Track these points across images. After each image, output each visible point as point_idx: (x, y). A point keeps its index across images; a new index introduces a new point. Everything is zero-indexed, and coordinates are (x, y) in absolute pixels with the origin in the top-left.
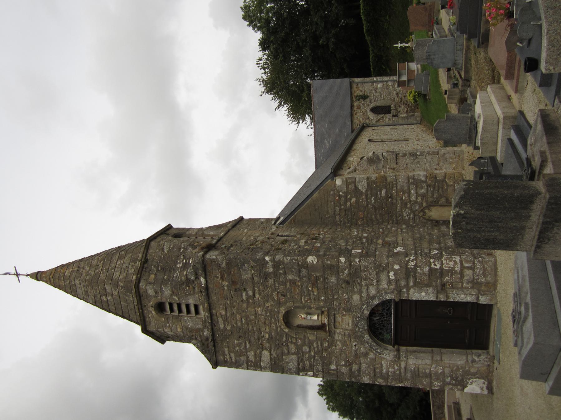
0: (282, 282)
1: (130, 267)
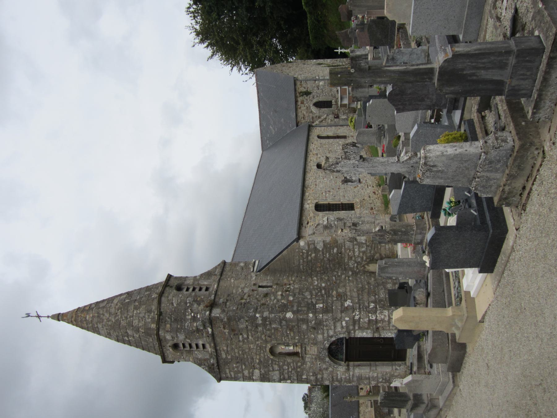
0: (269, 329)
1: (146, 316)
